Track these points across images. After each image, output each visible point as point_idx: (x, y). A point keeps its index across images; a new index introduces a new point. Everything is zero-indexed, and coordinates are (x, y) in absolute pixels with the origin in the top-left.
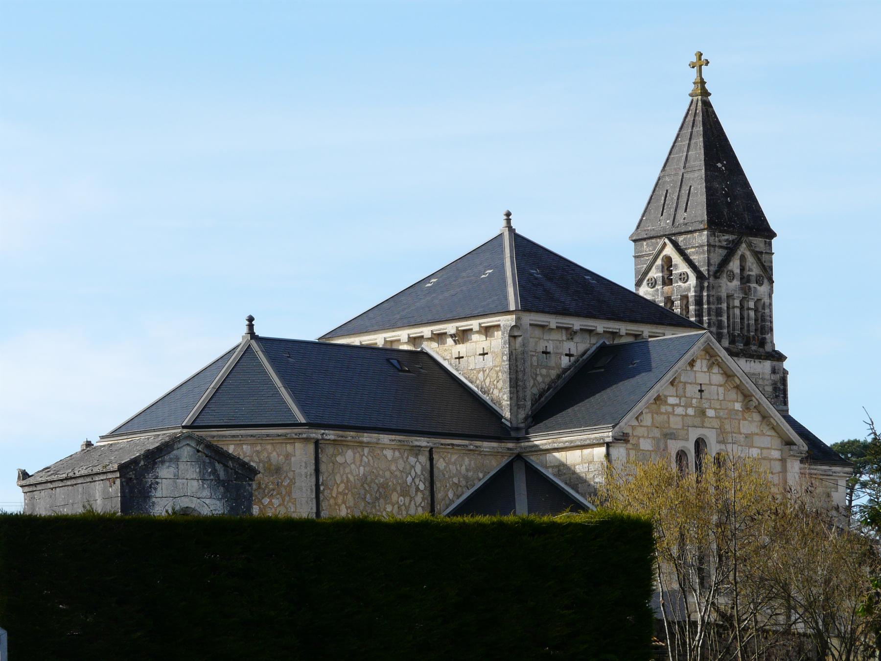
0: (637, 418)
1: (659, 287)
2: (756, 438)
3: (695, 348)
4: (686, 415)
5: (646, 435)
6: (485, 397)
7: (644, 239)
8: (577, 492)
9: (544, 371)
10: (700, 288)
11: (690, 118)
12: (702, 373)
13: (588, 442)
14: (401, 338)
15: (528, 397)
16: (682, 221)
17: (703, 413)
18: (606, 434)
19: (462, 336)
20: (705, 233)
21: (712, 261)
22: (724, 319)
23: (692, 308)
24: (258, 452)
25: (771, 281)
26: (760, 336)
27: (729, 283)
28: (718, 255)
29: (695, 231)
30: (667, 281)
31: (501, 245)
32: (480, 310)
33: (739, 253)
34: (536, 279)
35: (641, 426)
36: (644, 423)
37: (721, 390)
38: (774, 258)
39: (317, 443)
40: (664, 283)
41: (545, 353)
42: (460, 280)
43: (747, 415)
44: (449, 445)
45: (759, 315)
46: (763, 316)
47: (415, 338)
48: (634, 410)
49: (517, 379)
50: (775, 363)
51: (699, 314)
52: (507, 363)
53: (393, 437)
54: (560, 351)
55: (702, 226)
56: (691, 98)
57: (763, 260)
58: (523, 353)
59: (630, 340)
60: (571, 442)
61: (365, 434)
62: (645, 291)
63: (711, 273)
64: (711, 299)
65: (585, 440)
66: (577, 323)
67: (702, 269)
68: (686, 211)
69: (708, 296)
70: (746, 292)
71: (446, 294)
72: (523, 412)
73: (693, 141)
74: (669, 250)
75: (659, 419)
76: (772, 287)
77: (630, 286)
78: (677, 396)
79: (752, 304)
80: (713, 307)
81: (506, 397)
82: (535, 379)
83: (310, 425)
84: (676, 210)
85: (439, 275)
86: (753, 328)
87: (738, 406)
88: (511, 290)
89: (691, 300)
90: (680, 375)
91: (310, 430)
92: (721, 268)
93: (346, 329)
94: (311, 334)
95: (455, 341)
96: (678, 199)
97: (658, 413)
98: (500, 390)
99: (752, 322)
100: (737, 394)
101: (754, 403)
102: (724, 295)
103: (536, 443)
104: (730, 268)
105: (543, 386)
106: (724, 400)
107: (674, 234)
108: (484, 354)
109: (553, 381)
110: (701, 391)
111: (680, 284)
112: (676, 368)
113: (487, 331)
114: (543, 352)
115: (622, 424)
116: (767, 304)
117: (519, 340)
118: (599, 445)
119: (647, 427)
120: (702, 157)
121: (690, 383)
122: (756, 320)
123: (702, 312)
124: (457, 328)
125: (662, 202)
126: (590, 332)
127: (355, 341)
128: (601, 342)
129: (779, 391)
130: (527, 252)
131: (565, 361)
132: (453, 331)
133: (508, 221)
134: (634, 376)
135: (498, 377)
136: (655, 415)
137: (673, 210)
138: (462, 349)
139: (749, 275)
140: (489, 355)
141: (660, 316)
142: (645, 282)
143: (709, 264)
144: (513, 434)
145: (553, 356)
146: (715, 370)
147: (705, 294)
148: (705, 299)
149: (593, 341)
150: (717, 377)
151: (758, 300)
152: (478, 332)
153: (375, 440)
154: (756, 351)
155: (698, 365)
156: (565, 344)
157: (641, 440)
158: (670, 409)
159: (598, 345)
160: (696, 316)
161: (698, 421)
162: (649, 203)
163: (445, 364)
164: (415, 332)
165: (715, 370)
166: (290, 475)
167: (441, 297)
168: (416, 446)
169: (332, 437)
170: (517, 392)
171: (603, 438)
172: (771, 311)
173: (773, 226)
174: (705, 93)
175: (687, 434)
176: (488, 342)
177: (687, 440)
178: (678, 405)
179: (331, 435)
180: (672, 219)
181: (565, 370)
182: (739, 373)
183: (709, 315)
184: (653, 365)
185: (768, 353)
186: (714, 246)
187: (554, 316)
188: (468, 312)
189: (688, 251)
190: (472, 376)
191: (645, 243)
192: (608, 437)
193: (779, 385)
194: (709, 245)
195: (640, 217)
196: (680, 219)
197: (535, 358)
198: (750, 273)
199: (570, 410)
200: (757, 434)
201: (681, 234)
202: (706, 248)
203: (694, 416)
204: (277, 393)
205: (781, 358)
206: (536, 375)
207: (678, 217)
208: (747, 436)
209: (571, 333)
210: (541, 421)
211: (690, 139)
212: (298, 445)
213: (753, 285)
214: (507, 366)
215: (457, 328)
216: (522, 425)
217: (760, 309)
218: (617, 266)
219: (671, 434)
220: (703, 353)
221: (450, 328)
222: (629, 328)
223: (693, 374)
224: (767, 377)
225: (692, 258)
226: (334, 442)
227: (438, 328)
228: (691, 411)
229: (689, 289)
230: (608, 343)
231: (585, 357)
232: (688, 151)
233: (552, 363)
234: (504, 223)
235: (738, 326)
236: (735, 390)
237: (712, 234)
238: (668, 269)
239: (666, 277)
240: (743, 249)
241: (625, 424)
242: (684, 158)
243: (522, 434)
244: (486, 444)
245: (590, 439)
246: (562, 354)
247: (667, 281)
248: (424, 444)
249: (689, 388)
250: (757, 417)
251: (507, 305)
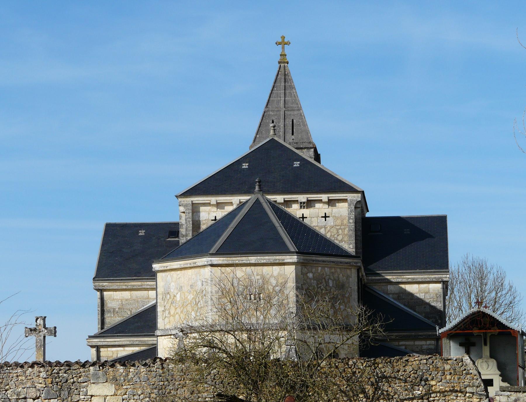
8: (415, 311)
13: (428, 280)
19: (309, 204)
24: (332, 272)
29: (305, 148)
60: (414, 279)
68: (293, 134)
162: (259, 127)
166: (349, 289)
171: (441, 278)
209: (219, 205)
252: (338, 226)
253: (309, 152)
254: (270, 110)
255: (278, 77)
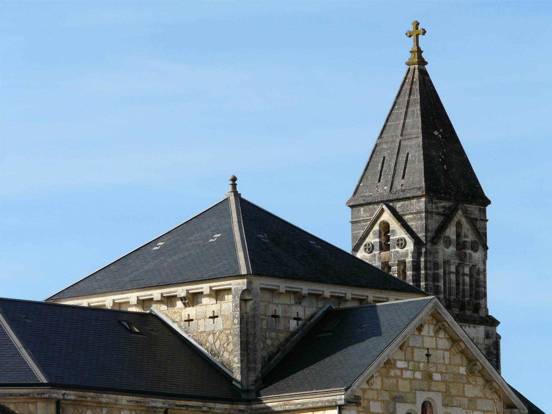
0: (368, 382)
1: (376, 252)
2: (479, 401)
3: (423, 313)
4: (414, 379)
5: (375, 398)
6: (216, 360)
7: (362, 205)
9: (273, 335)
10: (417, 253)
11: (407, 87)
12: (429, 338)
13: (320, 404)
14: (131, 300)
15: (259, 360)
16: (399, 188)
17: (429, 377)
18: (338, 397)
19: (193, 299)
20: (423, 199)
21: (429, 228)
22: (441, 284)
23: (409, 273)
25: (486, 248)
26: (475, 302)
27: (446, 250)
28: (436, 221)
30: (385, 246)
31: (228, 209)
32: (211, 274)
33: (456, 219)
34: (264, 243)
35: (372, 389)
36: (374, 387)
37: (447, 354)
38: (488, 224)
39: (58, 403)
40: (381, 249)
41: (275, 316)
42: (188, 244)
43: (471, 379)
44: (183, 406)
45: (474, 280)
46: (478, 281)
47: (144, 301)
48: (366, 374)
49: (247, 342)
50: (488, 328)
51: (417, 279)
52: (238, 326)
53: (131, 398)
54: (288, 315)
55: (420, 193)
56: (407, 67)
57: (478, 226)
58: (254, 316)
59: (355, 304)
60: (303, 404)
61: (104, 395)
62: (361, 255)
63: (429, 239)
64: (428, 265)
65: (317, 402)
66: (305, 288)
67: (420, 235)
68: (403, 177)
69: (426, 261)
70: (462, 257)
71: (175, 258)
72: (253, 375)
73: (410, 109)
74: (387, 216)
75: (388, 382)
76: (486, 253)
77: (348, 249)
78: (405, 360)
79: (467, 270)
80: (430, 272)
81: (237, 359)
82: (264, 342)
83: (52, 385)
84: (393, 177)
85: (165, 238)
86: (467, 294)
87: (462, 370)
88: (241, 255)
89: (409, 265)
90: (408, 339)
91: (52, 391)
92: (437, 235)
93: (74, 290)
94: (40, 296)
95: (184, 304)
96: (395, 166)
97: (388, 376)
98: (231, 353)
99: (467, 288)
100: (462, 358)
101: (479, 367)
102: (440, 260)
103: (269, 405)
104: (447, 234)
105: (272, 349)
106: (450, 364)
107: (392, 201)
108: (214, 317)
109: (282, 345)
110: (428, 355)
111: (398, 249)
112: (405, 333)
113: (218, 294)
114: (273, 316)
115: (354, 387)
116: (482, 270)
117: (250, 303)
118: (331, 407)
119: (377, 390)
120: (420, 125)
121: (418, 348)
122: (471, 286)
123: (420, 277)
124: (187, 291)
125: (379, 168)
126: (317, 296)
127: (84, 302)
128: (328, 306)
129: (493, 353)
130: (255, 218)
131: (293, 325)
132: (183, 294)
133: (234, 186)
134: (363, 341)
135: (228, 339)
136: (385, 379)
137: (390, 177)
138: (191, 311)
139: (465, 242)
140: (220, 318)
141: (380, 279)
142: (362, 248)
143: (427, 230)
144: (244, 396)
145: (282, 320)
146: (442, 334)
147: (422, 259)
148: (422, 265)
149: (320, 305)
150: (443, 342)
151: (473, 266)
152: (208, 296)
153: (113, 401)
154: (470, 316)
155: (425, 332)
156: (294, 308)
157: (372, 403)
158: (398, 373)
159: (325, 309)
160: (413, 281)
161: (425, 385)
163: (175, 326)
164: (144, 294)
165: (442, 334)
167: (169, 260)
168: (153, 407)
169: (73, 397)
170: (248, 354)
171: (335, 401)
172: (485, 277)
173: (487, 194)
174: (422, 62)
175: (415, 397)
176: (219, 305)
177: (414, 403)
178: (407, 369)
179: (72, 395)
180: (389, 185)
181: (293, 334)
182: (464, 338)
183: (426, 280)
184: (383, 329)
185: (481, 318)
186: (432, 213)
187: (283, 280)
188: (199, 276)
189: (406, 218)
190: (202, 338)
191: (362, 209)
192: (341, 399)
193: (492, 349)
194: (427, 212)
195: (356, 183)
196: (397, 186)
197: (264, 322)
198: (466, 239)
199: (300, 373)
200: (480, 398)
201: (399, 200)
202: (424, 215)
203: (422, 380)
204: (18, 354)
205: (494, 323)
206: (266, 338)
207: (396, 183)
208: (471, 400)
209: (299, 298)
210: (272, 384)
211: (407, 107)
212: (40, 405)
213: (469, 251)
214: (238, 329)
215: (187, 291)
216: (253, 387)
217: (475, 275)
218: (334, 228)
219: (400, 397)
220: (431, 318)
221: (181, 291)
222: (354, 293)
223: (421, 338)
224: (481, 341)
225: (409, 224)
226: (75, 403)
227: (168, 291)
228: (418, 375)
229: (406, 255)
230: (334, 307)
231: (312, 321)
232: (405, 119)
233: (281, 327)
234: (230, 188)
235: (454, 292)
236: (460, 355)
237: (429, 201)
238: (385, 235)
239: (383, 242)
240: (459, 216)
241: (358, 386)
242: (401, 126)
243: (253, 396)
244: (218, 406)
245: (322, 402)
246: (290, 318)
247: (384, 246)
248: (160, 405)
249: (416, 352)
250: (480, 381)
251: (239, 269)
252: (227, 329)
253: (419, 203)
254: (384, 141)
255: (404, 88)
